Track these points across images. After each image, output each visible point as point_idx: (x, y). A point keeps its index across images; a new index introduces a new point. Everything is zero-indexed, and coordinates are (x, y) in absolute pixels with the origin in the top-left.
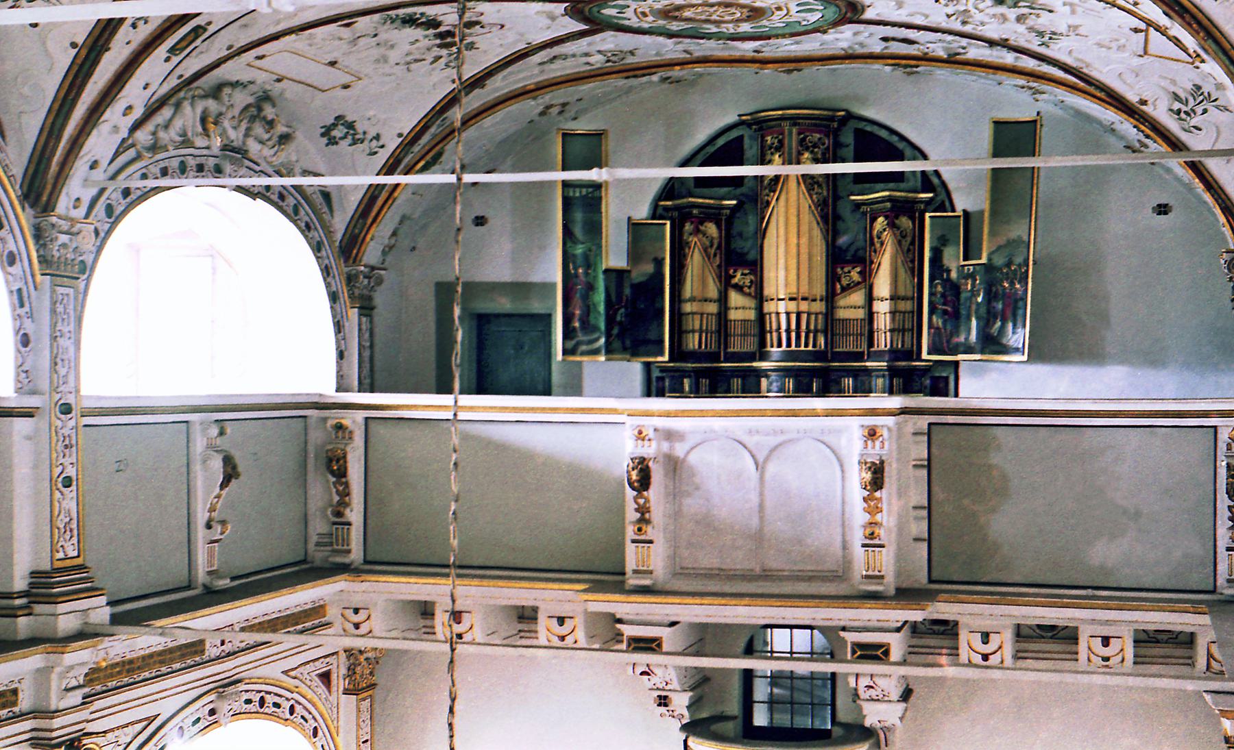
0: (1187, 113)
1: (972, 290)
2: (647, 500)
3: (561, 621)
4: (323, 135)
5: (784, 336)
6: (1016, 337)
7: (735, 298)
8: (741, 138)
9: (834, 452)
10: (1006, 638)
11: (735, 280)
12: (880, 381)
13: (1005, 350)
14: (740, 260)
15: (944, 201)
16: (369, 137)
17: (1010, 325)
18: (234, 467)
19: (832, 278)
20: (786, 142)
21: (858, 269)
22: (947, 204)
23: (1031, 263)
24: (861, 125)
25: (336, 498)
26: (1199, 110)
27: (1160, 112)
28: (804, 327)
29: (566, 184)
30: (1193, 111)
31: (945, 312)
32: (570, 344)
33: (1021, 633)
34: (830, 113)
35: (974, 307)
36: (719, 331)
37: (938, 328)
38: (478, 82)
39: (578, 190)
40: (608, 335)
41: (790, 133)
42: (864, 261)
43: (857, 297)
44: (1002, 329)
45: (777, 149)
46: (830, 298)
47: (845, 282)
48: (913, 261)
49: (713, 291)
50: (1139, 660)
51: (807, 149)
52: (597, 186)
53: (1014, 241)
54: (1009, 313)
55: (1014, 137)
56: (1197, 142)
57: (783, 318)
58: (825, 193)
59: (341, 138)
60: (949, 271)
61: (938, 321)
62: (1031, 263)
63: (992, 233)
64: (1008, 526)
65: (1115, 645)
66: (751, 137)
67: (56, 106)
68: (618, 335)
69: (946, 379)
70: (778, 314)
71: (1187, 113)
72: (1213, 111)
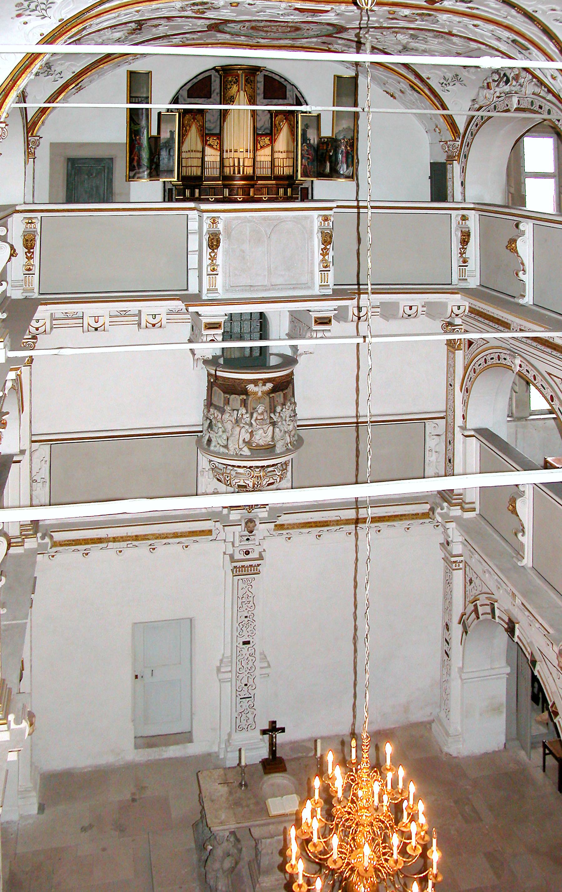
0: (446, 85)
1: (327, 149)
2: (216, 254)
6: (348, 171)
7: (208, 150)
8: (211, 75)
16: (56, 73)
18: (15, 251)
21: (268, 138)
24: (267, 73)
26: (451, 84)
28: (241, 164)
30: (449, 84)
31: (308, 158)
33: (472, 311)
35: (327, 157)
36: (293, 166)
43: (268, 151)
45: (234, 83)
46: (255, 150)
47: (262, 144)
49: (200, 148)
57: (236, 160)
60: (310, 140)
65: (158, 318)
66: (215, 76)
68: (155, 168)
70: (239, 159)
71: (446, 85)
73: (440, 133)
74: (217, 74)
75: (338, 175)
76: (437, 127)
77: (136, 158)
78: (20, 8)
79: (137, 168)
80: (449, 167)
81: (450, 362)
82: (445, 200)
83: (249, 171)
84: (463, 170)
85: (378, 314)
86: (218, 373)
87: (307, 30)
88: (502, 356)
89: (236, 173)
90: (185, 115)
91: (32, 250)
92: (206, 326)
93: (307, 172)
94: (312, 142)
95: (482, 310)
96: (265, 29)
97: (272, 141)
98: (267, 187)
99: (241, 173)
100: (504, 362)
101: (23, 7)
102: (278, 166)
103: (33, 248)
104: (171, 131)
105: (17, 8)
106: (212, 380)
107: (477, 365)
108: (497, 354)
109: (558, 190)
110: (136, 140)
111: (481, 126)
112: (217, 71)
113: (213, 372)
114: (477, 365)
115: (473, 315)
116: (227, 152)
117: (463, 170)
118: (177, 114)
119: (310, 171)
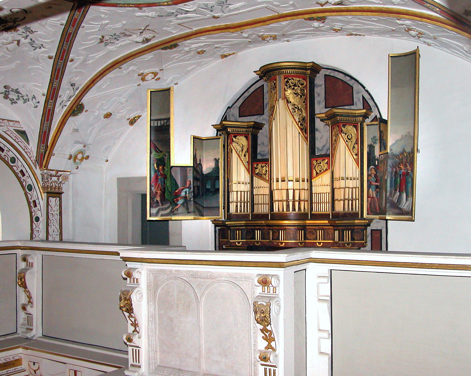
5: (291, 204)
6: (408, 203)
8: (263, 85)
11: (257, 171)
14: (258, 160)
17: (404, 195)
24: (328, 72)
37: (373, 198)
42: (329, 157)
43: (325, 178)
49: (248, 180)
57: (291, 192)
58: (304, 115)
61: (373, 193)
68: (183, 204)
83: (304, 206)
89: (285, 210)
93: (376, 208)
97: (330, 165)
98: (323, 229)
102: (267, 204)
104: (215, 159)
109: (302, 249)
111: (19, 179)
116: (277, 181)
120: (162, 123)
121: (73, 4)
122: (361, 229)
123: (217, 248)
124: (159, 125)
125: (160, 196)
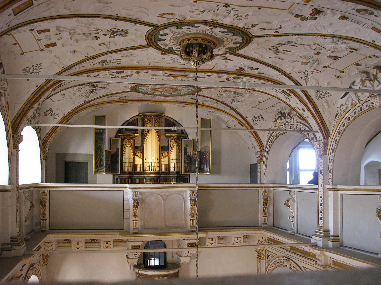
0: (256, 121)
2: (137, 210)
3: (107, 242)
4: (44, 113)
6: (207, 169)
7: (137, 159)
8: (137, 119)
9: (181, 196)
10: (83, 244)
12: (173, 180)
13: (204, 172)
14: (139, 149)
15: (186, 137)
16: (55, 114)
18: (33, 205)
19: (160, 154)
20: (151, 121)
21: (167, 152)
22: (187, 137)
23: (210, 152)
25: (42, 212)
26: (259, 120)
27: (250, 120)
29: (96, 129)
30: (257, 120)
32: (97, 170)
34: (161, 114)
38: (89, 102)
39: (98, 130)
40: (106, 167)
41: (153, 118)
43: (167, 159)
44: (204, 167)
46: (160, 159)
48: (180, 151)
50: (219, 243)
51: (156, 122)
52: (103, 129)
53: (206, 146)
54: (205, 163)
55: (205, 123)
56: (256, 127)
59: (48, 114)
60: (188, 153)
62: (210, 152)
63: (201, 144)
64: (214, 216)
66: (140, 119)
67: (26, 103)
69: (187, 179)
71: (256, 121)
72: (261, 120)
73: (254, 148)
74: (140, 118)
75: (202, 171)
76: (253, 145)
77: (98, 161)
78: (25, 71)
79: (99, 167)
80: (258, 165)
81: (259, 267)
82: (256, 183)
84: (266, 166)
85: (223, 243)
86: (140, 272)
87: (181, 90)
88: (283, 261)
90: (124, 140)
91: (45, 207)
92: (139, 247)
93: (187, 170)
94: (189, 154)
95: (274, 239)
96: (159, 90)
97: (169, 154)
99: (153, 170)
100: (283, 264)
101: (26, 71)
103: (45, 206)
105: (24, 72)
106: (137, 276)
107: (271, 267)
108: (280, 260)
110: (98, 152)
111: (273, 142)
112: (140, 116)
113: (138, 271)
114: (271, 267)
115: (269, 242)
117: (266, 166)
118: (120, 139)
119: (188, 170)
120: (100, 130)
121: (146, 43)
122: (143, 178)
123: (115, 182)
124: (99, 131)
125: (99, 163)
